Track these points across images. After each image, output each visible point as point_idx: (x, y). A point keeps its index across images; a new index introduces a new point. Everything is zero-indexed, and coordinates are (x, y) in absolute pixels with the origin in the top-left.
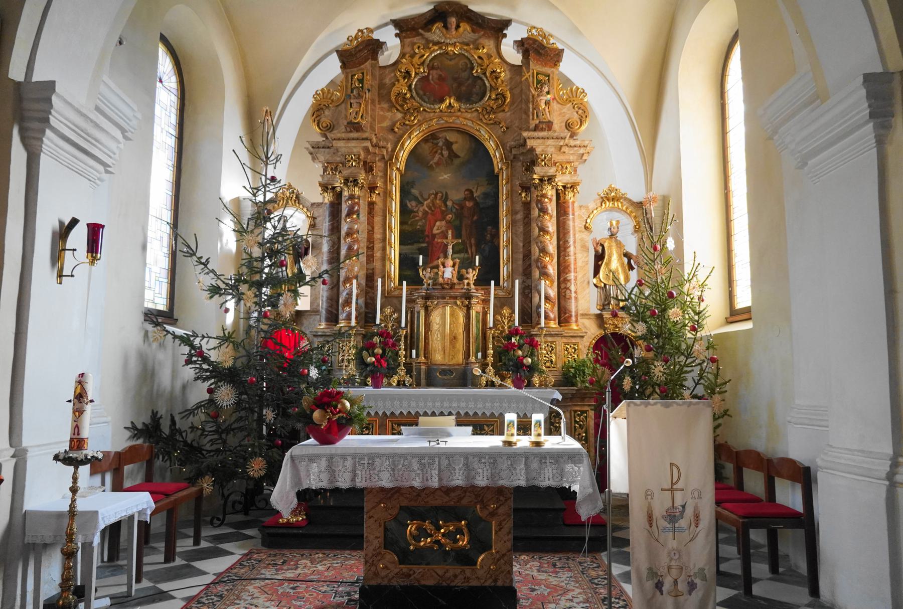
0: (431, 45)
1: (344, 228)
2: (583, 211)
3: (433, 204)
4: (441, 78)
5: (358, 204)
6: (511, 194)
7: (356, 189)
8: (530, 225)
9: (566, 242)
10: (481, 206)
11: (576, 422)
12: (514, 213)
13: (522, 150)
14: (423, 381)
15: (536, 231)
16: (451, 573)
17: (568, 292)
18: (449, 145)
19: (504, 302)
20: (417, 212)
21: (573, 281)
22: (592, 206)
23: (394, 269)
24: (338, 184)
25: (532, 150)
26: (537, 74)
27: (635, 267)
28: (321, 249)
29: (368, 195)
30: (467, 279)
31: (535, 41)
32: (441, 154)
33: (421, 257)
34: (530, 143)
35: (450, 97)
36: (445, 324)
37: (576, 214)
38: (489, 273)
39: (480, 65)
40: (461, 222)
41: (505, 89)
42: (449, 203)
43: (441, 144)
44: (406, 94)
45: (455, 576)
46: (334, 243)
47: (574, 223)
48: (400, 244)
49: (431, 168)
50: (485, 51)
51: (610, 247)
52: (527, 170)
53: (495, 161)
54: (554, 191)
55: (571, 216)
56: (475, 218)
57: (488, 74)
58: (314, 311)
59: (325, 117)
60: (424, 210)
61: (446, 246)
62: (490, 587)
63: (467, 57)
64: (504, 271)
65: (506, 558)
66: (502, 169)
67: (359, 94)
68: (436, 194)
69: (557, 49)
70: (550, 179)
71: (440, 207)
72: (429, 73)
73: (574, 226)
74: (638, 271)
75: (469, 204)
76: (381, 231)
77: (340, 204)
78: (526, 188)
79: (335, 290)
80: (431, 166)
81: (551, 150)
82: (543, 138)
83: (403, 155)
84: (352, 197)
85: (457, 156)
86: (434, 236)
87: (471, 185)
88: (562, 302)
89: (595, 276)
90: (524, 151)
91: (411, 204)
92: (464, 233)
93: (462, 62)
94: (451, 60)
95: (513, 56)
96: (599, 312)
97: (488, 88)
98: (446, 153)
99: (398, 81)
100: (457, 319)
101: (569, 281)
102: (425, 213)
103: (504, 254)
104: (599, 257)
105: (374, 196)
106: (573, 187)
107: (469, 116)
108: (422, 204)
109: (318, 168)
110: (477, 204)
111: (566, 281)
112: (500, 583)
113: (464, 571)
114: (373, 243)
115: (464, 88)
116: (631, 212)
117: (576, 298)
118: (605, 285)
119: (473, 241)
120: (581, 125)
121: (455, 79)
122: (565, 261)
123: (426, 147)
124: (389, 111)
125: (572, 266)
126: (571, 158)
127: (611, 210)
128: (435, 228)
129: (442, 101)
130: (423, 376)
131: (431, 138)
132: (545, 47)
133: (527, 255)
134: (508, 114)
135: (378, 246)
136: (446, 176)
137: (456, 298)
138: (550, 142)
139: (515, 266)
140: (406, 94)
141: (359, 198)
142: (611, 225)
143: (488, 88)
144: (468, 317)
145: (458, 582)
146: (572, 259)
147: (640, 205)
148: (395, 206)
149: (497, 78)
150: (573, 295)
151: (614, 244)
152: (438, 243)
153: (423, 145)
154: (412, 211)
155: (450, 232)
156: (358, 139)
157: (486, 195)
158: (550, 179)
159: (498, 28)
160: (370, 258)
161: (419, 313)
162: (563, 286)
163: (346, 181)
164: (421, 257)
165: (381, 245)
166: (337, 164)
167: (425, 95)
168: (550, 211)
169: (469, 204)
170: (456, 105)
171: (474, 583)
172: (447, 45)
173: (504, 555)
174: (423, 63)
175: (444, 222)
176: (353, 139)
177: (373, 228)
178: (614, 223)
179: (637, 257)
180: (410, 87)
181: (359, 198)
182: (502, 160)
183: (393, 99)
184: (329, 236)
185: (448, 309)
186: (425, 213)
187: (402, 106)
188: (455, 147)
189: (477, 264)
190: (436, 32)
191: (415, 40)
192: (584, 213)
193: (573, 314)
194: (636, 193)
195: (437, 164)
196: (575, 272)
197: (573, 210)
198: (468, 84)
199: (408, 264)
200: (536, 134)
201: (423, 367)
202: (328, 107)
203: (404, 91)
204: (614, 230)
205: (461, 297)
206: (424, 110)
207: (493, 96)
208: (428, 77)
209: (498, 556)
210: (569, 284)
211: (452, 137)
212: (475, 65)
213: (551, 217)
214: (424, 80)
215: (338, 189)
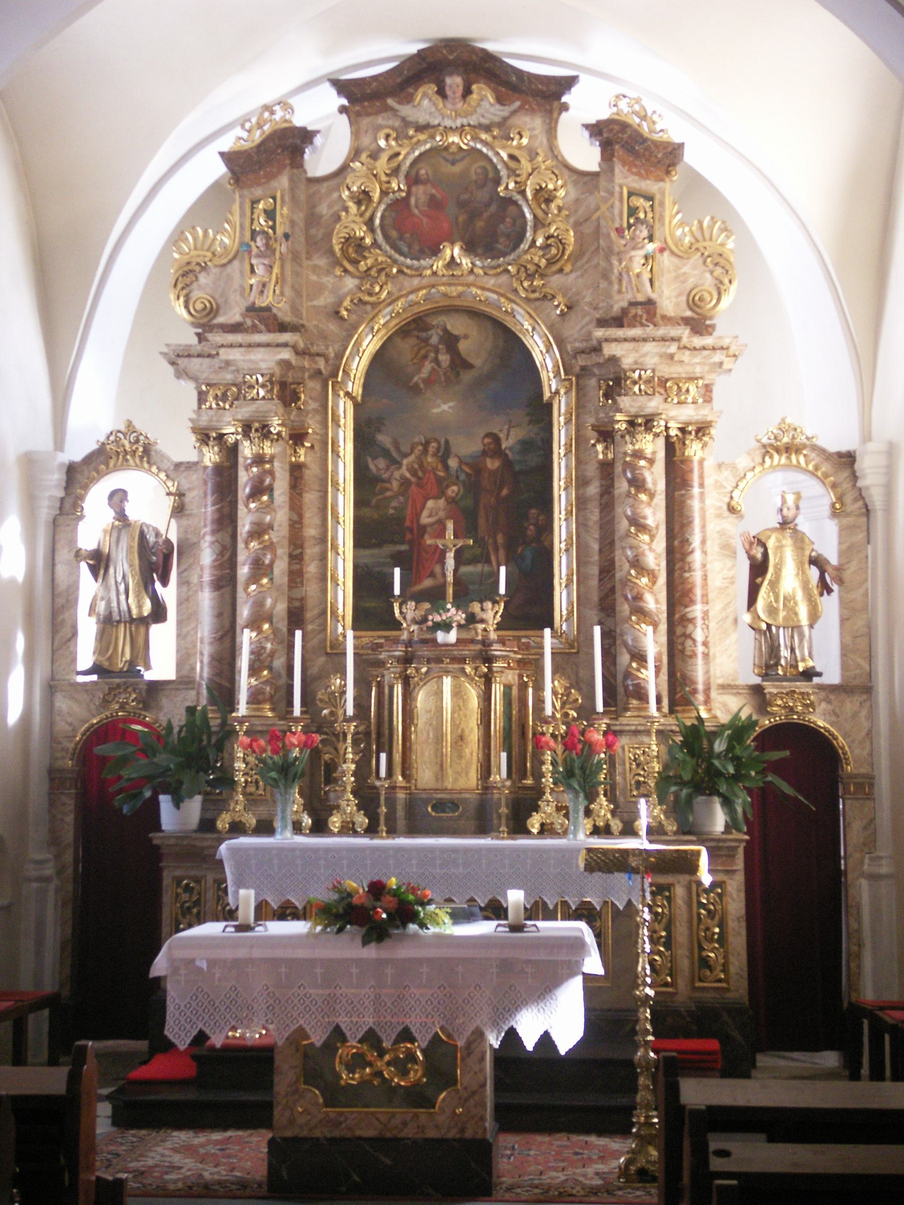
0: (411, 132)
1: (245, 525)
2: (726, 473)
3: (421, 466)
4: (434, 203)
5: (271, 473)
6: (579, 443)
7: (267, 443)
8: (613, 509)
9: (686, 542)
10: (517, 468)
11: (701, 905)
12: (582, 482)
13: (595, 359)
14: (401, 823)
15: (623, 525)
16: (396, 1122)
17: (689, 642)
18: (451, 341)
19: (571, 659)
20: (388, 481)
21: (699, 622)
22: (743, 462)
23: (343, 596)
24: (231, 431)
25: (614, 360)
26: (630, 194)
27: (835, 587)
28: (197, 558)
29: (289, 451)
30: (482, 621)
31: (624, 126)
32: (436, 361)
33: (397, 571)
34: (609, 350)
35: (453, 244)
36: (448, 711)
37: (708, 482)
38: (530, 608)
39: (513, 173)
40: (476, 502)
41: (562, 226)
42: (453, 463)
43: (434, 340)
44: (363, 238)
45: (405, 1124)
46: (224, 547)
47: (705, 504)
48: (355, 546)
49: (415, 390)
50: (525, 141)
51: (780, 548)
52: (607, 396)
53: (544, 375)
54: (661, 441)
55: (696, 490)
56: (505, 492)
57: (529, 194)
58: (185, 681)
59: (200, 288)
60: (402, 476)
61: (443, 554)
62: (454, 1140)
63: (486, 157)
64: (563, 599)
65: (477, 1097)
66: (557, 392)
67: (267, 245)
68: (426, 445)
69: (668, 144)
70: (649, 422)
71: (434, 469)
72: (409, 193)
73: (703, 510)
74: (841, 599)
75: (492, 464)
76: (317, 521)
77: (234, 465)
78: (606, 435)
79: (227, 640)
80: (416, 385)
81: (651, 361)
82: (634, 340)
83: (359, 366)
84: (259, 460)
85: (468, 366)
86: (423, 529)
87: (497, 426)
88: (678, 662)
89: (749, 609)
90: (601, 360)
91: (377, 465)
92: (482, 521)
93: (476, 167)
94: (453, 163)
95: (585, 155)
96: (757, 680)
97: (530, 224)
98: (445, 358)
99: (346, 209)
100: (465, 701)
101: (692, 621)
102: (405, 483)
103: (563, 565)
104: (758, 569)
105: (302, 451)
106: (702, 430)
107: (491, 282)
108: (399, 465)
109: (188, 390)
110: (507, 463)
111: (687, 620)
112: (468, 1134)
113: (416, 1116)
114: (302, 546)
115: (480, 224)
116: (826, 476)
117: (706, 655)
118: (769, 626)
119: (500, 539)
120: (719, 300)
121: (462, 205)
122: (684, 581)
123: (406, 347)
124: (328, 273)
125: (698, 592)
126: (698, 370)
127: (789, 466)
128: (425, 513)
129: (435, 252)
130: (400, 813)
131: (414, 326)
132: (645, 140)
133: (607, 569)
134: (573, 276)
135: (311, 551)
136: (445, 407)
137: (462, 660)
138: (649, 347)
139: (582, 589)
140: (363, 238)
141: (271, 461)
142: (784, 501)
143: (530, 224)
144: (486, 698)
145: (409, 1132)
146: (697, 576)
147: (848, 459)
148: (345, 471)
149: (548, 201)
150: (700, 649)
151: (788, 542)
152: (430, 546)
153: (398, 341)
154: (378, 480)
155: (450, 525)
156: (268, 345)
157: (526, 445)
158: (649, 422)
159: (549, 94)
160: (296, 576)
161: (391, 688)
162: (679, 630)
163: (247, 429)
164: (397, 571)
165: (317, 550)
166: (227, 386)
167: (401, 238)
168: (650, 485)
169: (492, 464)
170: (466, 262)
171: (432, 1134)
172: (448, 130)
173: (474, 1093)
174: (395, 172)
175: (442, 502)
176: (259, 345)
177: (301, 516)
178: (790, 499)
179: (839, 569)
180: (370, 223)
181: (273, 457)
182: (557, 374)
183: (337, 248)
184: (213, 532)
185: (447, 682)
186: (405, 483)
187: (355, 262)
188: (463, 346)
189: (502, 590)
190: (424, 105)
191: (380, 120)
192: (727, 478)
193: (700, 687)
194: (835, 434)
195: (428, 382)
196: (706, 601)
197: (701, 477)
198: (488, 219)
199: (370, 584)
200: (620, 333)
201: (401, 795)
202: (204, 268)
203: (359, 233)
204: (789, 514)
205: (474, 659)
206: (400, 271)
207: (540, 242)
208: (406, 200)
209: (465, 1095)
210: (690, 627)
211: (457, 325)
212: (503, 173)
213: (652, 496)
214: (399, 206)
215: (231, 440)
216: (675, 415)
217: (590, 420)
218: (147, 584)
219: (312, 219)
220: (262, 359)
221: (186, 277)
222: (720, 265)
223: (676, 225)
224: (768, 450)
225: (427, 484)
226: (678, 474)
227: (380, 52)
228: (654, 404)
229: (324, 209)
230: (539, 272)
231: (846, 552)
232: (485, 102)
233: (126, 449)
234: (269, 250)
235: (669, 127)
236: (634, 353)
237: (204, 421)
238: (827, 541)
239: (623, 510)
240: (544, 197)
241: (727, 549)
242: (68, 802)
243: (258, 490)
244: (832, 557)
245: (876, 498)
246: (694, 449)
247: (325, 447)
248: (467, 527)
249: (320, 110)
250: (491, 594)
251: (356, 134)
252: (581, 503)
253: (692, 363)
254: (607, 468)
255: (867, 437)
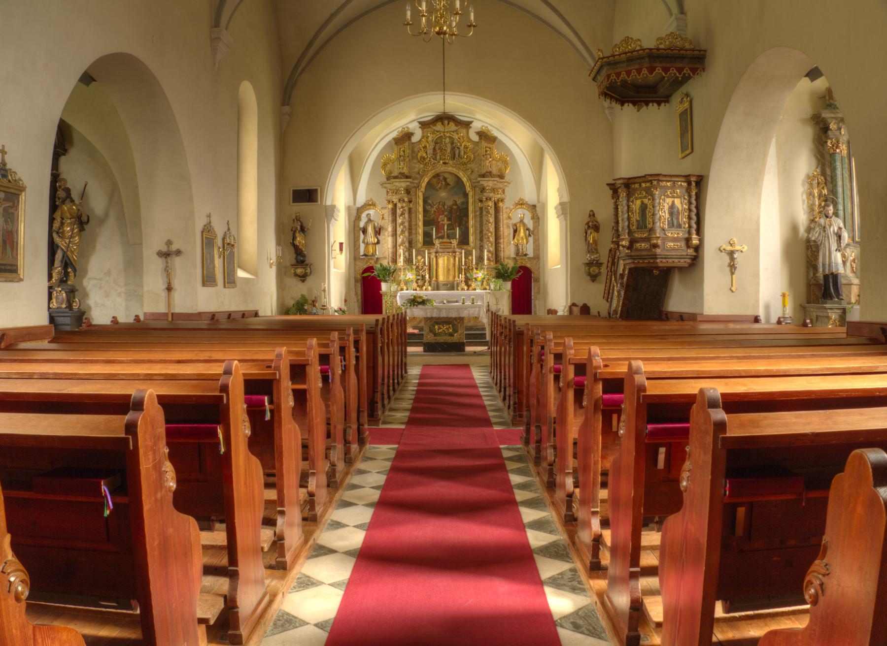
12: (475, 212)
15: (485, 222)
18: (445, 179)
22: (512, 207)
23: (420, 238)
24: (395, 201)
38: (464, 241)
47: (503, 216)
49: (437, 190)
64: (471, 239)
78: (481, 201)
83: (424, 185)
84: (402, 207)
87: (456, 198)
91: (428, 208)
95: (475, 138)
103: (471, 231)
104: (515, 231)
109: (385, 191)
111: (499, 243)
123: (435, 181)
131: (437, 176)
135: (413, 227)
147: (534, 206)
148: (421, 209)
157: (463, 203)
163: (400, 200)
169: (455, 207)
188: (448, 180)
190: (439, 127)
211: (446, 175)
216: (496, 197)
217: (477, 197)
218: (376, 235)
219: (413, 152)
220: (402, 184)
221: (385, 165)
222: (506, 163)
223: (496, 154)
224: (517, 204)
225: (440, 212)
226: (497, 210)
227: (428, 116)
228: (491, 195)
229: (416, 149)
230: (465, 164)
231: (535, 227)
232: (452, 126)
233: (369, 204)
234: (404, 160)
235: (495, 133)
236: (488, 183)
237: (389, 198)
238: (530, 225)
239: (485, 218)
240: (466, 147)
241: (508, 227)
242: (359, 285)
243: (402, 214)
244: (531, 228)
245: (540, 215)
246: (501, 204)
247: (416, 203)
248: (449, 219)
249: (414, 127)
250: (455, 238)
251: (423, 133)
252: (475, 216)
253: (501, 185)
254: (481, 209)
255: (539, 201)
